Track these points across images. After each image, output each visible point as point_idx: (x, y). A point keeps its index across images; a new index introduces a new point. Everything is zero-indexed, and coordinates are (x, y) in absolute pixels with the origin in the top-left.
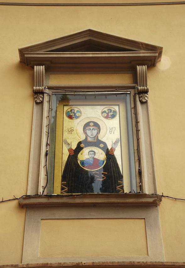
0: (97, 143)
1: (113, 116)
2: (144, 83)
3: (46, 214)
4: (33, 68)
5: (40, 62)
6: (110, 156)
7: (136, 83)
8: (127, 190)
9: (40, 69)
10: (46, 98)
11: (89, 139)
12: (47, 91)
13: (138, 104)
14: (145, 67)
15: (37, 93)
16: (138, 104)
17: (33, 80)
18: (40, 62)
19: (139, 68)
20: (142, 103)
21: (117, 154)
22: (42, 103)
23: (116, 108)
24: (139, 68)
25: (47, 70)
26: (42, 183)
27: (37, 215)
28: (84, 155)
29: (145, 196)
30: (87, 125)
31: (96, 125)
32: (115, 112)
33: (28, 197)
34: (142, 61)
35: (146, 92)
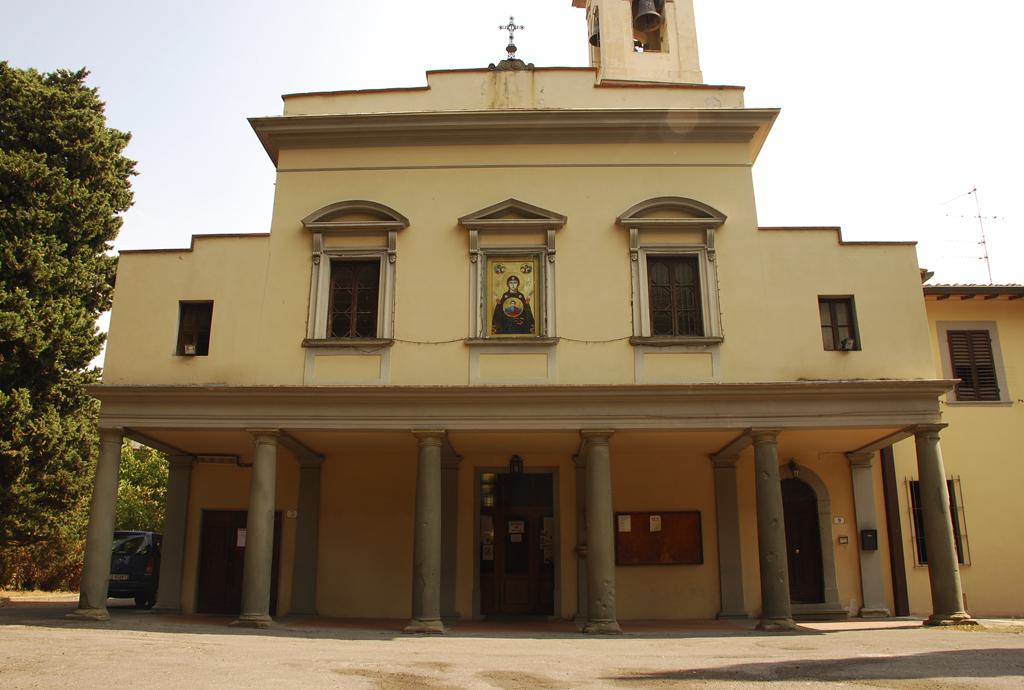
0: (517, 294)
1: (529, 271)
2: (712, 245)
3: (483, 350)
4: (388, 235)
5: (474, 228)
6: (527, 306)
7: (547, 244)
8: (550, 336)
9: (474, 233)
10: (479, 259)
11: (511, 291)
12: (480, 252)
13: (548, 263)
14: (553, 232)
15: (316, 257)
16: (548, 263)
17: (470, 243)
18: (474, 228)
19: (549, 232)
20: (391, 263)
21: (531, 304)
22: (637, 260)
23: (531, 264)
24: (549, 232)
25: (323, 236)
26: (479, 328)
27: (641, 350)
28: (507, 305)
29: (548, 339)
30: (510, 279)
31: (516, 279)
32: (530, 267)
33: (470, 339)
34: (711, 226)
35: (554, 253)
